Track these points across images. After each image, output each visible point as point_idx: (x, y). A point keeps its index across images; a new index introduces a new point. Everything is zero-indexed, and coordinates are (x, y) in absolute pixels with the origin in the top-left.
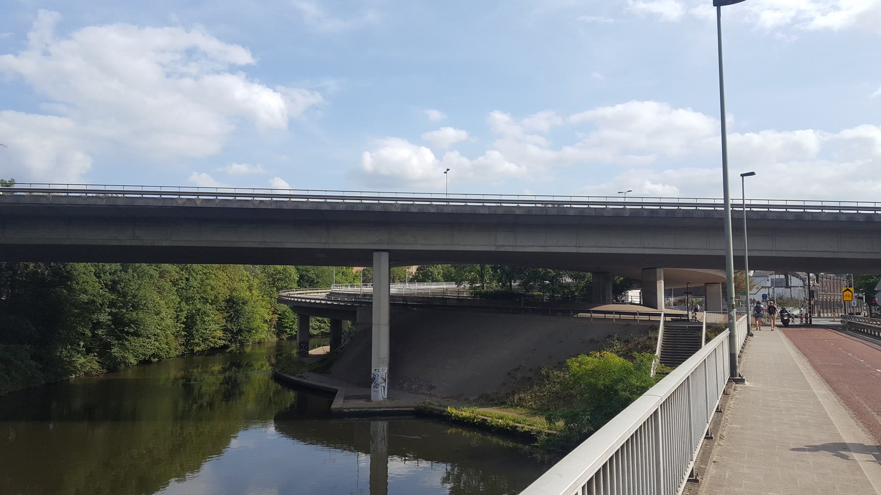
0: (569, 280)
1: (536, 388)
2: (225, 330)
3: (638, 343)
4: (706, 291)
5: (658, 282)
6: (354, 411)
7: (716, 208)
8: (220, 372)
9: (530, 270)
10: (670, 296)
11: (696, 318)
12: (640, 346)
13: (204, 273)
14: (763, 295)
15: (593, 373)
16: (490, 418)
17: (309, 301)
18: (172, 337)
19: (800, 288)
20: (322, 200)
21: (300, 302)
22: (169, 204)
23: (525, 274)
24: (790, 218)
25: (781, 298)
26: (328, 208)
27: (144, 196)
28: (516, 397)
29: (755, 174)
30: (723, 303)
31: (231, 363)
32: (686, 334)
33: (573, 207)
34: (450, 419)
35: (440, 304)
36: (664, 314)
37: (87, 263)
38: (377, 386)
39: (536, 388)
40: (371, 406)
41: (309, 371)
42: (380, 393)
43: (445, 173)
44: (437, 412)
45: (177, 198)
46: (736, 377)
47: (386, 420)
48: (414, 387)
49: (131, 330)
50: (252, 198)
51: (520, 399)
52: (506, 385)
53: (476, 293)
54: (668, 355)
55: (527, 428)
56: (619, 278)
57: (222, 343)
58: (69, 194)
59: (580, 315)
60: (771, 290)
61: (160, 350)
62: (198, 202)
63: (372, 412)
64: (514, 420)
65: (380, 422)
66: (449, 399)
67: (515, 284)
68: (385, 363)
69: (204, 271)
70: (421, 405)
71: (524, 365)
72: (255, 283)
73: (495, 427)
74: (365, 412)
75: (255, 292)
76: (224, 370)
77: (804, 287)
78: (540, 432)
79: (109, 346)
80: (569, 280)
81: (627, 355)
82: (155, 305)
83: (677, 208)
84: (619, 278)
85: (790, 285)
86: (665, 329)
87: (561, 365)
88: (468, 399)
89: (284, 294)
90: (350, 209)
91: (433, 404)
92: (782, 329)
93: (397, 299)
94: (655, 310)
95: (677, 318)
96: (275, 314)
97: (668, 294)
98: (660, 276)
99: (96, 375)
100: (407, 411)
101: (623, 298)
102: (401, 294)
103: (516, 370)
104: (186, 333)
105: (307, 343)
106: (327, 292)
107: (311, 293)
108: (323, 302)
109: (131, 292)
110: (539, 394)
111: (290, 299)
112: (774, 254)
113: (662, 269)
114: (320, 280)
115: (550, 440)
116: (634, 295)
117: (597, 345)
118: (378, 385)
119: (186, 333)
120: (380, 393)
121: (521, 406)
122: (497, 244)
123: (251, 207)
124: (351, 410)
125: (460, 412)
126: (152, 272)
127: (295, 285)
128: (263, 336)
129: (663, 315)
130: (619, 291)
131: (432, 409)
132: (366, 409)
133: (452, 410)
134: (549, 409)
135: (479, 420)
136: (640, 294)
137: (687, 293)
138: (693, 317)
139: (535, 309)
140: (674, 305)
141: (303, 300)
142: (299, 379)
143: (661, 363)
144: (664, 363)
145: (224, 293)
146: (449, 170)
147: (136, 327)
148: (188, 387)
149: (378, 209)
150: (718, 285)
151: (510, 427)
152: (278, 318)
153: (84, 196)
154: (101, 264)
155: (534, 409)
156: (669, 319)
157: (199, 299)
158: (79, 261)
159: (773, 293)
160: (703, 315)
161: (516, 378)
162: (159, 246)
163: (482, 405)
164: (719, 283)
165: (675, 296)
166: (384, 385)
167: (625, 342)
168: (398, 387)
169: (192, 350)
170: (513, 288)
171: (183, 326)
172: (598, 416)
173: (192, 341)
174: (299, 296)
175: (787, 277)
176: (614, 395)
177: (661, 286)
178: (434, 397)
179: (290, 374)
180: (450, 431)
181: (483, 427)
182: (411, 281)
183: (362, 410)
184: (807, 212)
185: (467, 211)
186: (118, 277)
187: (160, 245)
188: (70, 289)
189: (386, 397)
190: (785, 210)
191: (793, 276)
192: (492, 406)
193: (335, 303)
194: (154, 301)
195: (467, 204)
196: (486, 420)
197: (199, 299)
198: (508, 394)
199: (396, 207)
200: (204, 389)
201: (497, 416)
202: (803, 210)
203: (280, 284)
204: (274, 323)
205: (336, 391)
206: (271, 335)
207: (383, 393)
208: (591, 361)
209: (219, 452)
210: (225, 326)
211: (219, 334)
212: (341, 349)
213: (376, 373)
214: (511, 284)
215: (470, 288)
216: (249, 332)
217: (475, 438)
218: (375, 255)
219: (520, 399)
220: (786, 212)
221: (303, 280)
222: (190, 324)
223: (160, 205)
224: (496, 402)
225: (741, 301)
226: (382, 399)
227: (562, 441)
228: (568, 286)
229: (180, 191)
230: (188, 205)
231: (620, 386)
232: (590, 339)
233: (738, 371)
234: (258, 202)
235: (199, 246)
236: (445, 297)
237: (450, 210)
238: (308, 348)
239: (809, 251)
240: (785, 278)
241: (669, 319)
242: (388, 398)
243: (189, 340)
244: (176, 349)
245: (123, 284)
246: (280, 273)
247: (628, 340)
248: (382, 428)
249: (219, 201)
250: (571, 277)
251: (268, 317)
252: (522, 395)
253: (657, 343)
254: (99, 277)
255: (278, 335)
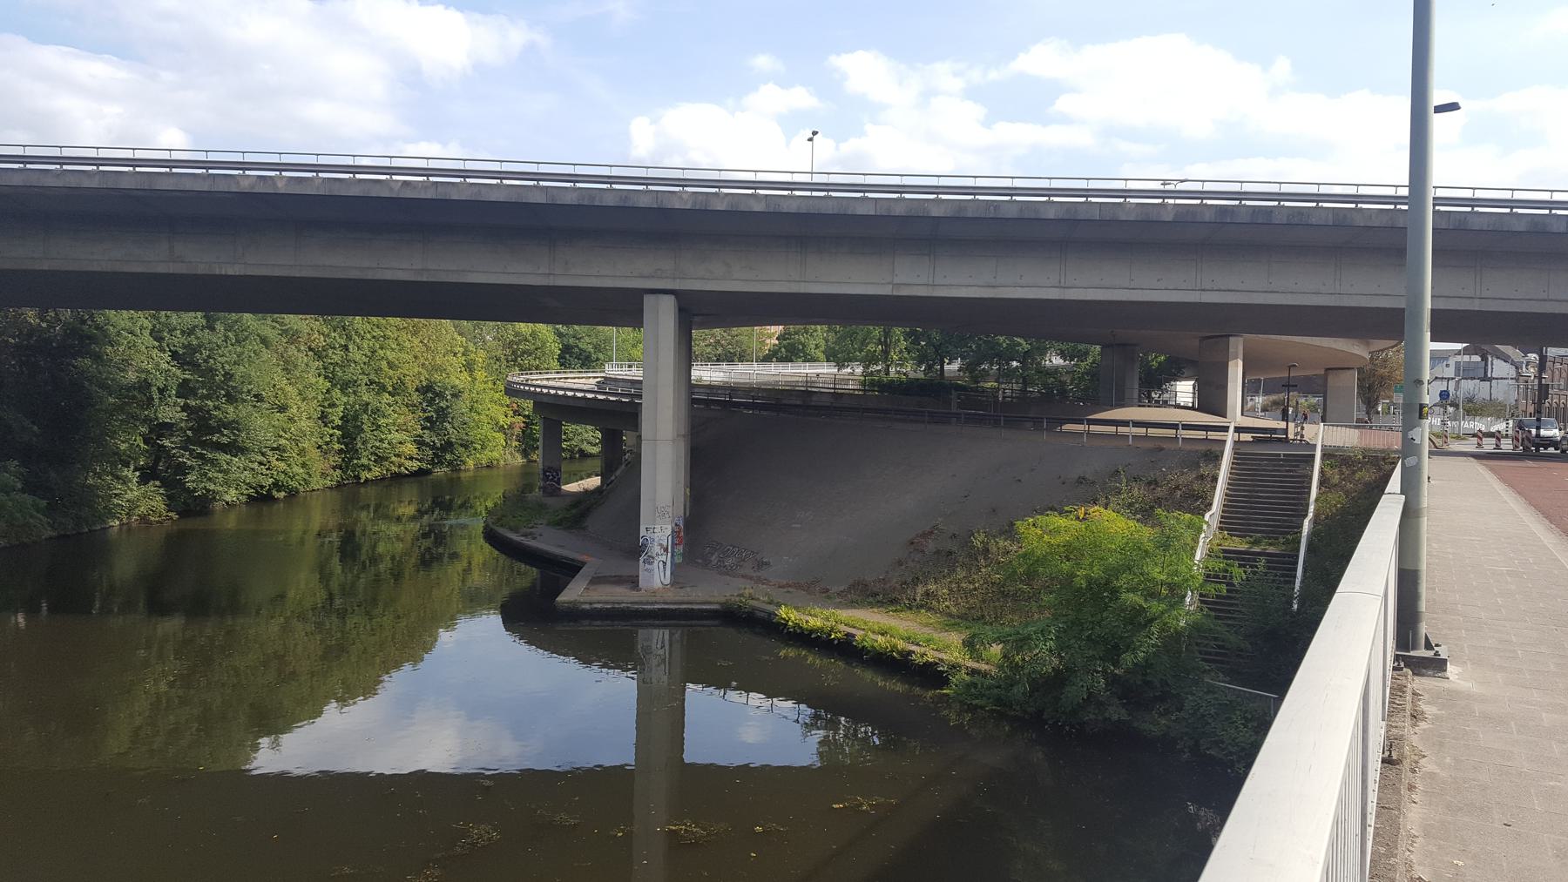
0: (1057, 361)
1: (961, 573)
2: (420, 443)
3: (1177, 487)
4: (1325, 385)
5: (1230, 363)
6: (601, 609)
7: (1359, 205)
8: (413, 518)
9: (980, 339)
10: (1256, 392)
11: (1302, 436)
12: (1179, 492)
13: (374, 337)
14: (1442, 392)
15: (1070, 551)
16: (862, 632)
17: (563, 392)
18: (315, 454)
19: (1510, 382)
20: (531, 183)
21: (533, 392)
22: (222, 187)
23: (971, 347)
24: (1521, 227)
25: (1470, 400)
26: (540, 199)
27: (174, 170)
28: (920, 590)
29: (1459, 108)
30: (1358, 407)
31: (433, 502)
32: (1278, 471)
33: (1053, 202)
34: (785, 631)
35: (798, 403)
36: (1235, 428)
37: (137, 312)
38: (650, 560)
39: (961, 573)
40: (636, 599)
41: (548, 525)
42: (657, 575)
43: (810, 140)
44: (762, 614)
45: (239, 175)
46: (1414, 648)
47: (665, 626)
48: (729, 562)
49: (225, 440)
50: (388, 177)
51: (927, 594)
52: (901, 565)
53: (870, 384)
54: (1237, 513)
55: (931, 656)
56: (1156, 357)
57: (414, 465)
58: (28, 166)
59: (1068, 427)
60: (1452, 384)
61: (289, 477)
62: (280, 184)
63: (637, 611)
64: (908, 639)
65: (656, 631)
66: (790, 589)
67: (952, 367)
68: (667, 516)
69: (375, 334)
70: (733, 599)
71: (940, 527)
72: (480, 357)
73: (869, 651)
74: (623, 610)
75: (480, 375)
76: (421, 513)
77: (1517, 380)
78: (955, 667)
79: (182, 469)
80: (1057, 361)
81: (1145, 514)
82: (277, 394)
83: (1276, 203)
84: (1156, 357)
85: (1489, 376)
86: (1234, 458)
87: (1009, 532)
88: (827, 591)
89: (516, 379)
90: (586, 203)
91: (758, 599)
92: (1485, 462)
93: (720, 392)
94: (1224, 420)
95: (1266, 437)
96: (519, 415)
97: (1250, 388)
98: (1237, 353)
99: (158, 522)
100: (706, 610)
101: (1166, 396)
102: (727, 382)
103: (925, 535)
104: (343, 447)
105: (558, 471)
106: (597, 377)
107: (575, 378)
108: (590, 396)
109: (223, 367)
110: (964, 585)
111: (527, 388)
112: (1476, 306)
113: (1241, 339)
114: (601, 356)
115: (975, 685)
116: (1184, 390)
117: (1089, 491)
118: (653, 558)
119: (343, 447)
120: (657, 575)
121: (929, 609)
122: (895, 282)
123: (387, 194)
124: (596, 606)
125: (804, 618)
126: (268, 332)
127: (555, 363)
128: (496, 455)
129: (1231, 430)
130: (1154, 383)
131: (754, 609)
132: (624, 605)
133: (788, 614)
134: (983, 616)
135: (839, 635)
136: (1194, 388)
137: (1289, 386)
138: (1296, 434)
139: (979, 415)
140: (1263, 410)
141: (545, 391)
142: (523, 538)
143: (1221, 528)
144: (1227, 529)
145: (414, 374)
146: (817, 132)
147: (234, 434)
148: (349, 546)
149: (644, 202)
150: (1351, 372)
151: (899, 653)
152: (524, 422)
153: (56, 170)
154: (163, 313)
155: (950, 615)
156: (1247, 437)
157: (366, 384)
158: (118, 307)
159: (1456, 389)
160: (1319, 428)
161: (923, 551)
162: (221, 275)
163: (853, 604)
164: (1353, 368)
165: (1266, 393)
166: (664, 558)
167: (1150, 483)
168: (700, 561)
169: (358, 477)
170: (946, 375)
171: (338, 433)
172: (1072, 641)
173: (355, 462)
174: (545, 383)
175: (1484, 359)
176: (1111, 599)
177: (1236, 371)
178: (763, 584)
179: (511, 529)
180: (784, 651)
181: (846, 649)
182: (767, 359)
183: (617, 606)
184: (1555, 215)
185: (830, 209)
186: (198, 338)
187: (223, 273)
188: (97, 358)
189: (667, 581)
190: (1508, 210)
191: (1498, 358)
192: (871, 605)
193: (611, 398)
194: (274, 386)
195: (830, 193)
196: (853, 636)
197: (366, 384)
198: (905, 583)
199: (681, 197)
200: (381, 549)
201: (876, 627)
202: (1547, 212)
203: (526, 362)
204: (517, 431)
205: (584, 563)
206: (511, 454)
207: (662, 574)
208: (1062, 527)
209: (416, 659)
210: (419, 436)
211: (410, 449)
212: (608, 485)
213: (648, 535)
214: (942, 367)
215: (865, 374)
216: (465, 446)
217: (832, 671)
218: (648, 300)
219: (927, 594)
220: (1510, 214)
221: (571, 354)
222: (350, 431)
223: (206, 188)
224: (880, 597)
225: (1394, 404)
226: (660, 585)
227: (999, 687)
228: (1055, 371)
229: (245, 160)
230: (260, 189)
231: (1122, 581)
232: (1077, 477)
233: (1424, 628)
234: (400, 184)
235: (298, 275)
236: (809, 389)
237: (793, 208)
238: (559, 479)
239: (1552, 300)
240: (1482, 360)
241: (1247, 437)
242: (673, 583)
243: (351, 459)
244: (324, 475)
245: (205, 353)
246: (526, 340)
247: (1155, 480)
248: (660, 643)
249: (321, 181)
250: (1063, 355)
251: (502, 420)
252: (932, 587)
253: (1215, 488)
254: (160, 339)
255: (525, 453)
